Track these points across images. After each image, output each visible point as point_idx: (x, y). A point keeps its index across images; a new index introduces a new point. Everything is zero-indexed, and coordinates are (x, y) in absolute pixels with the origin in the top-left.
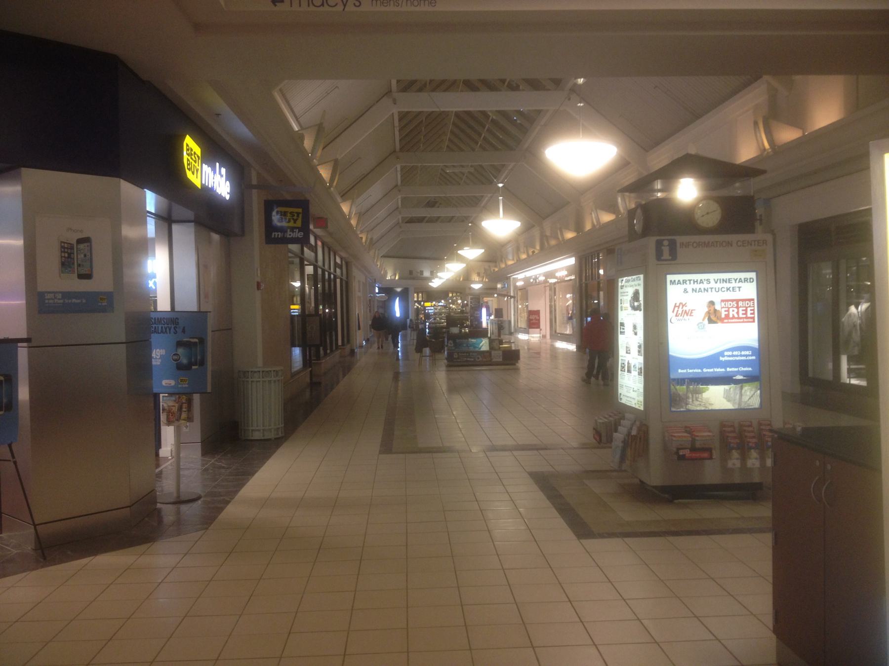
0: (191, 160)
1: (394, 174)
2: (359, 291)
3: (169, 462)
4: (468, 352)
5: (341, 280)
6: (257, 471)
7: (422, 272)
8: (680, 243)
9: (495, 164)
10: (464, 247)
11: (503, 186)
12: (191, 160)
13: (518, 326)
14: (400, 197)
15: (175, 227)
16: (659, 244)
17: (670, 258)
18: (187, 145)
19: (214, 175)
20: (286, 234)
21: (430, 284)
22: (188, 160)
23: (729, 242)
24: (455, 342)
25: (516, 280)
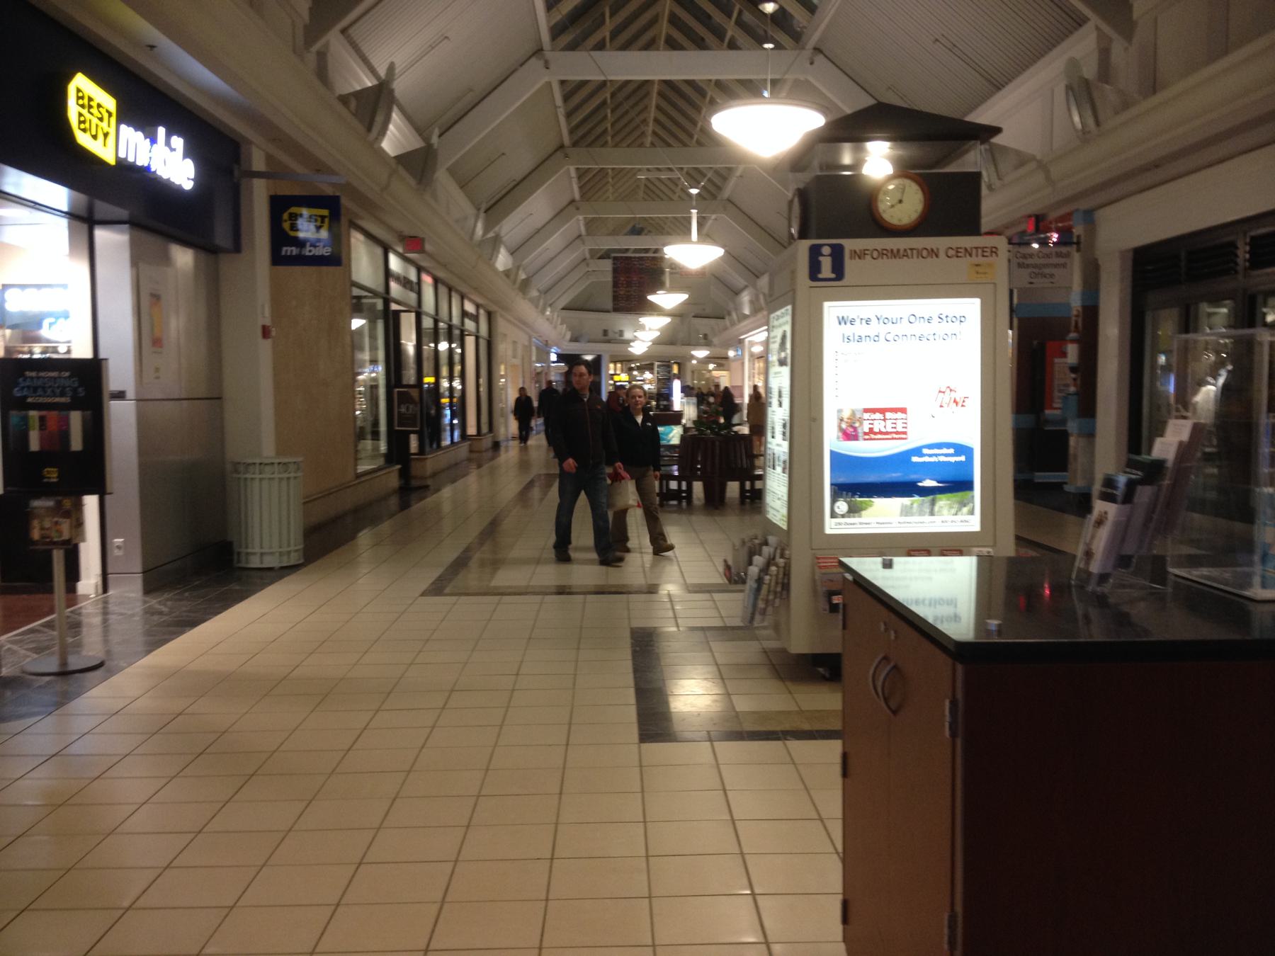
0: (88, 116)
1: (565, 181)
2: (514, 357)
5: (477, 338)
6: (210, 618)
7: (621, 333)
8: (851, 251)
11: (698, 194)
12: (88, 116)
14: (581, 217)
15: (101, 234)
16: (815, 252)
18: (79, 90)
21: (630, 349)
22: (80, 115)
23: (932, 250)
25: (752, 344)
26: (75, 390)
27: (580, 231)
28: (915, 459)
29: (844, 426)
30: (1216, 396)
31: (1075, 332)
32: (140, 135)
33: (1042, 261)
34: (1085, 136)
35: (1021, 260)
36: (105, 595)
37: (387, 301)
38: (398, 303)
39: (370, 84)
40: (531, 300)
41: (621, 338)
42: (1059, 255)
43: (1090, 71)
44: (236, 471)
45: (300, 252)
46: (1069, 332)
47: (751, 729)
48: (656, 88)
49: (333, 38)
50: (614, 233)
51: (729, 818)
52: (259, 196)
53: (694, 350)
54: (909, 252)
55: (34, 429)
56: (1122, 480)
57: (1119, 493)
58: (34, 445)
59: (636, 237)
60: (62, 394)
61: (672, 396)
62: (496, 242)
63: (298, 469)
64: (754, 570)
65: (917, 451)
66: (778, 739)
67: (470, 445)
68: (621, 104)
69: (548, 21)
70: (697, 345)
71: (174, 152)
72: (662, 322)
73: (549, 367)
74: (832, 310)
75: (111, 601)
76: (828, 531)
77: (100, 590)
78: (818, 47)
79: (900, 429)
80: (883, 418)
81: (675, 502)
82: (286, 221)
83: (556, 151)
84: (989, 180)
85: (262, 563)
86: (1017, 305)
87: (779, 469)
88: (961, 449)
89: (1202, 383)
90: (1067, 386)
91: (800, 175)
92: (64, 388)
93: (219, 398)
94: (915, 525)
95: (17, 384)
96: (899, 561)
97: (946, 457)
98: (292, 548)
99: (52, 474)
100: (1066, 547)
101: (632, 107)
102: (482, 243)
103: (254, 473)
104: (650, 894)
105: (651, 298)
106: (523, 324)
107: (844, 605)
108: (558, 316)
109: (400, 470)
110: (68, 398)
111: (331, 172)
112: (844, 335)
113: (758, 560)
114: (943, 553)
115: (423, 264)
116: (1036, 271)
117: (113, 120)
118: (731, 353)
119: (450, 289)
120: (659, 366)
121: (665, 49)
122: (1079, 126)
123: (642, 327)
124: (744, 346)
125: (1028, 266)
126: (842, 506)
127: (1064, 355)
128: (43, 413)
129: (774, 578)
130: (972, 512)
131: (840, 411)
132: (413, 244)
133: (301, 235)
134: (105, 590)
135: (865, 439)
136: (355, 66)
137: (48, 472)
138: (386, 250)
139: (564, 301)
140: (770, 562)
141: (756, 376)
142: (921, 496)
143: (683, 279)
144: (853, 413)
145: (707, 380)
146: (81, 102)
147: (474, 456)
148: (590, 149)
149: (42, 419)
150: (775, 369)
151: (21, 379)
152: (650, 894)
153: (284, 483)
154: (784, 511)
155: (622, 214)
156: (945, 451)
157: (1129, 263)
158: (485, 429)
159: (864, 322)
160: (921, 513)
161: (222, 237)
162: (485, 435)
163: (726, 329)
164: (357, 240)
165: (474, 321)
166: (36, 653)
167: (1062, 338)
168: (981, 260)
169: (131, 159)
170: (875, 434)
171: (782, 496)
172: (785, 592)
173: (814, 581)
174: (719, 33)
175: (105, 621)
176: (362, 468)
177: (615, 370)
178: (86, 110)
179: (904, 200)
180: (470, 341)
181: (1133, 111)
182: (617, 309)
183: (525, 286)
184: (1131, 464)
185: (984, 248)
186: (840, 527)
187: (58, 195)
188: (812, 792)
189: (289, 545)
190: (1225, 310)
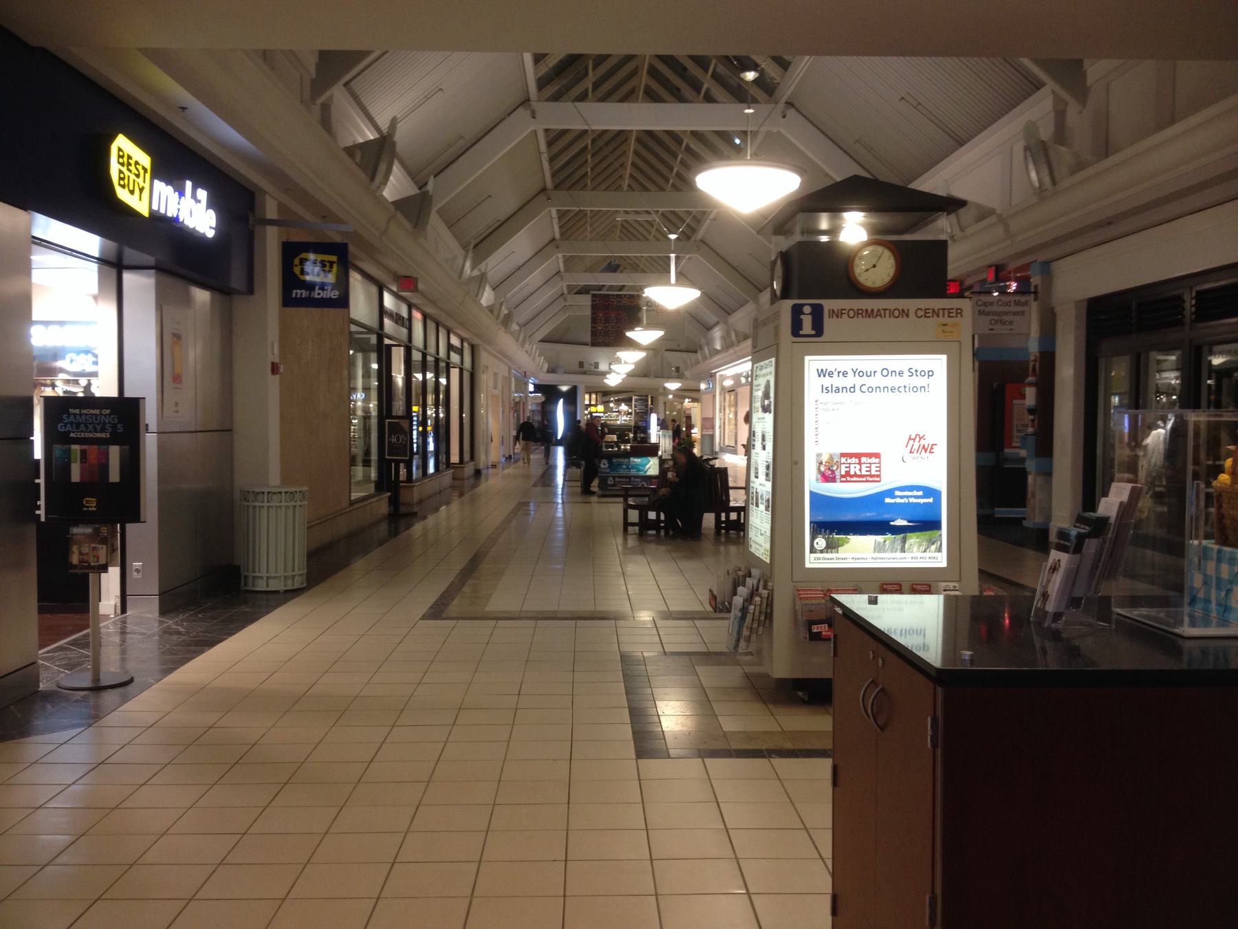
0: (127, 173)
1: (547, 221)
2: (495, 388)
3: (110, 621)
4: (629, 477)
5: (461, 370)
7: (597, 365)
8: (829, 310)
9: (676, 210)
10: (634, 328)
11: (677, 238)
12: (127, 173)
13: (724, 444)
14: (560, 255)
15: (128, 277)
16: (797, 311)
17: (813, 332)
18: (120, 150)
19: (180, 198)
20: (312, 292)
21: (605, 381)
22: (121, 172)
23: (903, 311)
24: (610, 463)
25: (723, 378)
26: (114, 427)
27: (559, 268)
28: (888, 500)
29: (822, 469)
30: (1165, 439)
31: (1032, 376)
32: (170, 188)
33: (1002, 309)
34: (1041, 192)
35: (982, 308)
36: (124, 615)
37: (380, 337)
38: (390, 338)
39: (372, 138)
40: (512, 334)
41: (596, 370)
42: (1017, 303)
43: (1046, 132)
44: (246, 499)
45: (310, 295)
46: (1027, 376)
47: (739, 747)
48: (634, 135)
49: (337, 93)
50: (590, 270)
51: (724, 827)
52: (271, 243)
53: (667, 382)
54: (882, 312)
55: (76, 462)
56: (1074, 532)
57: (1071, 545)
58: (76, 476)
59: (613, 274)
60: (103, 430)
61: (650, 429)
62: (482, 280)
63: (304, 497)
64: (738, 600)
65: (890, 493)
66: (764, 757)
67: (453, 473)
68: (601, 149)
69: (536, 73)
70: (670, 377)
71: (198, 204)
72: (638, 356)
73: (527, 397)
74: (813, 364)
75: (128, 621)
76: (808, 565)
77: (119, 611)
78: (789, 101)
79: (873, 472)
80: (858, 462)
81: (653, 532)
82: (296, 266)
83: (539, 193)
84: (952, 232)
85: (267, 586)
86: (977, 348)
87: (762, 507)
88: (929, 492)
89: (1154, 426)
90: (1026, 426)
91: (781, 239)
92: (105, 423)
93: (230, 430)
94: (887, 560)
95: (61, 420)
96: (882, 598)
97: (917, 499)
98: (297, 572)
99: (91, 504)
100: (1026, 581)
101: (611, 152)
102: (471, 279)
103: (263, 502)
104: (656, 893)
105: (629, 334)
106: (504, 356)
107: (835, 636)
108: (536, 349)
109: (390, 497)
110: (108, 434)
111: (339, 221)
112: (822, 386)
113: (743, 591)
114: (914, 591)
115: (414, 301)
116: (996, 318)
117: (148, 176)
118: (703, 386)
119: (438, 325)
120: (636, 401)
121: (643, 101)
122: (1037, 184)
123: (618, 361)
124: (715, 379)
125: (988, 314)
126: (821, 542)
127: (1023, 397)
128: (85, 447)
129: (758, 608)
130: (939, 550)
131: (819, 455)
132: (407, 283)
133: (308, 278)
134: (124, 610)
135: (842, 482)
136: (355, 115)
137: (87, 502)
138: (381, 288)
139: (541, 334)
140: (754, 592)
141: (727, 408)
142: (893, 535)
143: (658, 317)
144: (831, 457)
145: (679, 411)
146: (121, 160)
147: (457, 483)
148: (570, 192)
149: (83, 453)
150: (757, 415)
151: (64, 416)
152: (656, 893)
153: (291, 511)
154: (768, 546)
155: (598, 252)
156: (916, 493)
157: (1084, 311)
158: (467, 457)
159: (841, 374)
160: (893, 550)
161: (237, 279)
162: (467, 463)
163: (698, 363)
164: (355, 279)
165: (459, 354)
166: (68, 670)
167: (1020, 381)
168: (947, 320)
169: (162, 211)
170: (852, 476)
171: (765, 532)
172: (767, 621)
173: (795, 612)
174: (696, 86)
175: (123, 641)
176: (355, 496)
177: (590, 400)
178: (126, 167)
179: (877, 265)
180: (455, 373)
181: (1091, 171)
182: (594, 344)
183: (506, 321)
184: (1080, 520)
185: (949, 309)
186: (819, 561)
187: (91, 243)
188: (798, 806)
189: (293, 570)
190: (1173, 358)
